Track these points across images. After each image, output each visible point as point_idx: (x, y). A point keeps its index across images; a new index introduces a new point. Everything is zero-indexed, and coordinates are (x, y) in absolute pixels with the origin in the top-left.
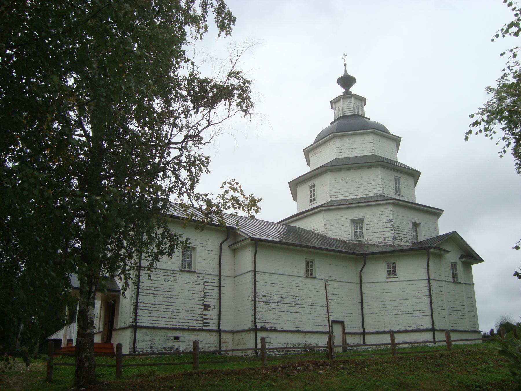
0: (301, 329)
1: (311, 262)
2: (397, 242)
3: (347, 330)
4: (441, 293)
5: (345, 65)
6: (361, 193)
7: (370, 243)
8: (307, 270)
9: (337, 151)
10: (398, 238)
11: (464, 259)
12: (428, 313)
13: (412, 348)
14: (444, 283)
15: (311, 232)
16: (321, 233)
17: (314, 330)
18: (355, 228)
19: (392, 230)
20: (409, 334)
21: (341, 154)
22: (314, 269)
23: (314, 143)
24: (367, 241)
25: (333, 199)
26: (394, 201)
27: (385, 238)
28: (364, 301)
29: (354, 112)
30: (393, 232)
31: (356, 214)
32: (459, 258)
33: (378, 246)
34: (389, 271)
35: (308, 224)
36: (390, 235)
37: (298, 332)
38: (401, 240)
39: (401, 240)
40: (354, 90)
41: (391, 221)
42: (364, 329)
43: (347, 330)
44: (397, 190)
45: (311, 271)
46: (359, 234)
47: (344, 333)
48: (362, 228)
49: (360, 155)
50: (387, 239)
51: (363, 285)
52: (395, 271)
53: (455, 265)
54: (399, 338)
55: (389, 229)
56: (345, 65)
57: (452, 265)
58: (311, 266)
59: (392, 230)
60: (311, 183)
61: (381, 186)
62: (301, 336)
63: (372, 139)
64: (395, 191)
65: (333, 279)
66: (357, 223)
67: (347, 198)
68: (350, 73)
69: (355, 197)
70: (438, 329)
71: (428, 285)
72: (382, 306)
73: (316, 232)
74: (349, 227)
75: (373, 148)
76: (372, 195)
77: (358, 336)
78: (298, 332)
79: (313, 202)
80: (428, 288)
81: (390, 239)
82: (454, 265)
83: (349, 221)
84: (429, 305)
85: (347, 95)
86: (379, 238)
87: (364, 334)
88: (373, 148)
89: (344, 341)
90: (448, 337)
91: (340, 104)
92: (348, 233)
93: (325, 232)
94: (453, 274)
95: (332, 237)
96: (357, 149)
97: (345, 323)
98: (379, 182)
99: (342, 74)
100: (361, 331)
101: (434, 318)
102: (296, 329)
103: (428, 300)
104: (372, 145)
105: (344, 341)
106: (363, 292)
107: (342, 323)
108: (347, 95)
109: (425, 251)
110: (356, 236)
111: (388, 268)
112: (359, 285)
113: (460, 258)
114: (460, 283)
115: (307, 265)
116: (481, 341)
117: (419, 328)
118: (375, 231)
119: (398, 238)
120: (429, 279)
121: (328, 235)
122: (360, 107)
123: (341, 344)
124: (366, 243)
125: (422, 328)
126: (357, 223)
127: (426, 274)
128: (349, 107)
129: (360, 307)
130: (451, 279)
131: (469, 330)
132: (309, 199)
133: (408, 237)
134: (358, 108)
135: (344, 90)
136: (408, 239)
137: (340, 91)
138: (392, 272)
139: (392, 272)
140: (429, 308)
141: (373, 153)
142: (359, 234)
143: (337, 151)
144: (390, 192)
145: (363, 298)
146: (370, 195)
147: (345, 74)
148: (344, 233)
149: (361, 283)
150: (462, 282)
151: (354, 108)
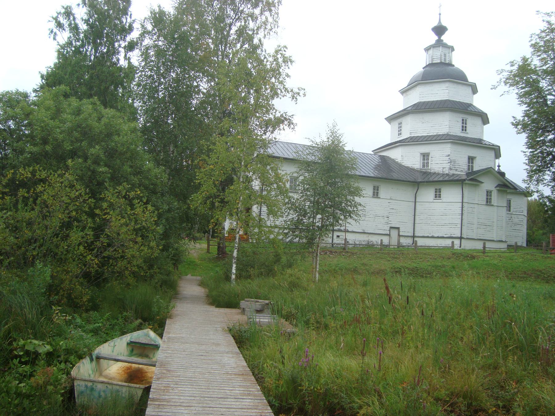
0: (366, 231)
1: (378, 187)
2: (452, 172)
3: (401, 234)
4: (472, 212)
5: (440, 14)
6: (433, 132)
7: (432, 171)
8: (374, 192)
9: (420, 96)
10: (454, 168)
11: (498, 188)
12: (459, 226)
13: (438, 249)
14: (476, 206)
15: (393, 160)
16: (399, 162)
17: (376, 232)
18: (424, 159)
19: (449, 162)
20: (444, 239)
21: (423, 98)
22: (379, 191)
23: (407, 86)
24: (431, 170)
25: (412, 135)
26: (452, 141)
27: (443, 168)
28: (416, 214)
29: (441, 60)
30: (449, 164)
31: (425, 149)
32: (495, 186)
33: (439, 174)
34: (436, 195)
35: (396, 155)
36: (447, 166)
37: (364, 233)
38: (456, 170)
39: (456, 170)
40: (445, 38)
41: (449, 156)
42: (414, 234)
43: (401, 234)
44: (464, 129)
45: (377, 193)
46: (425, 164)
47: (399, 236)
48: (428, 160)
49: (437, 100)
50: (445, 169)
51: (417, 203)
52: (440, 195)
53: (491, 192)
54: (488, 245)
55: (447, 162)
56: (440, 14)
57: (487, 192)
58: (378, 190)
59: (449, 162)
60: (399, 120)
61: (448, 126)
62: (365, 236)
63: (448, 86)
64: (461, 130)
65: (394, 198)
66: (425, 156)
67: (422, 135)
68: (444, 24)
69: (428, 134)
70: (465, 237)
71: (461, 206)
72: (429, 219)
73: (396, 161)
74: (419, 158)
75: (447, 94)
76: (441, 134)
77: (409, 238)
78: (364, 233)
79: (400, 136)
80: (461, 209)
81: (447, 169)
82: (489, 193)
83: (419, 155)
84: (460, 221)
85: (439, 43)
86: (439, 168)
87: (414, 237)
88: (447, 94)
89: (399, 241)
90: (484, 244)
91: (431, 52)
92: (417, 163)
93: (402, 162)
94: (487, 199)
95: (406, 165)
96: (435, 95)
97: (400, 229)
98: (447, 123)
99: (435, 24)
100: (412, 235)
101: (463, 230)
102: (363, 231)
103: (460, 217)
104: (447, 91)
105: (399, 241)
106: (416, 208)
107: (398, 228)
108: (439, 43)
109: (461, 182)
110: (424, 166)
111: (436, 192)
112: (414, 203)
113: (496, 187)
114: (493, 205)
115: (374, 189)
116: (506, 249)
117: (452, 235)
118: (437, 162)
119: (454, 168)
120: (462, 202)
121: (403, 164)
122: (447, 55)
123: (397, 244)
124: (429, 171)
125: (454, 236)
126: (425, 156)
127: (461, 198)
128: (437, 55)
129: (413, 219)
130: (485, 203)
131: (495, 240)
132: (397, 133)
133: (464, 167)
134: (445, 55)
135: (436, 38)
136: (462, 170)
137: (434, 38)
138: (438, 195)
139: (438, 195)
140: (460, 223)
141: (447, 99)
142: (425, 164)
143: (420, 96)
144: (457, 131)
145: (416, 212)
146: (439, 134)
147: (439, 23)
148: (415, 163)
149: (415, 202)
150: (495, 204)
151: (441, 55)
